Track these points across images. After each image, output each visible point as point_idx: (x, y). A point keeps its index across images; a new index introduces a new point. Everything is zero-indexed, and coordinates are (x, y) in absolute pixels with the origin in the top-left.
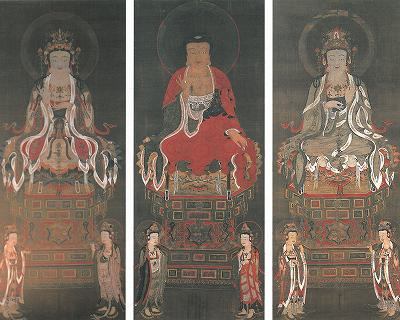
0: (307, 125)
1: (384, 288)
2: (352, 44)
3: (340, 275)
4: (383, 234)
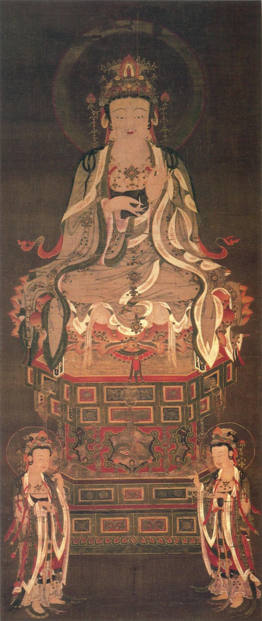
0: (70, 243)
1: (223, 556)
2: (160, 86)
3: (135, 531)
4: (220, 455)
